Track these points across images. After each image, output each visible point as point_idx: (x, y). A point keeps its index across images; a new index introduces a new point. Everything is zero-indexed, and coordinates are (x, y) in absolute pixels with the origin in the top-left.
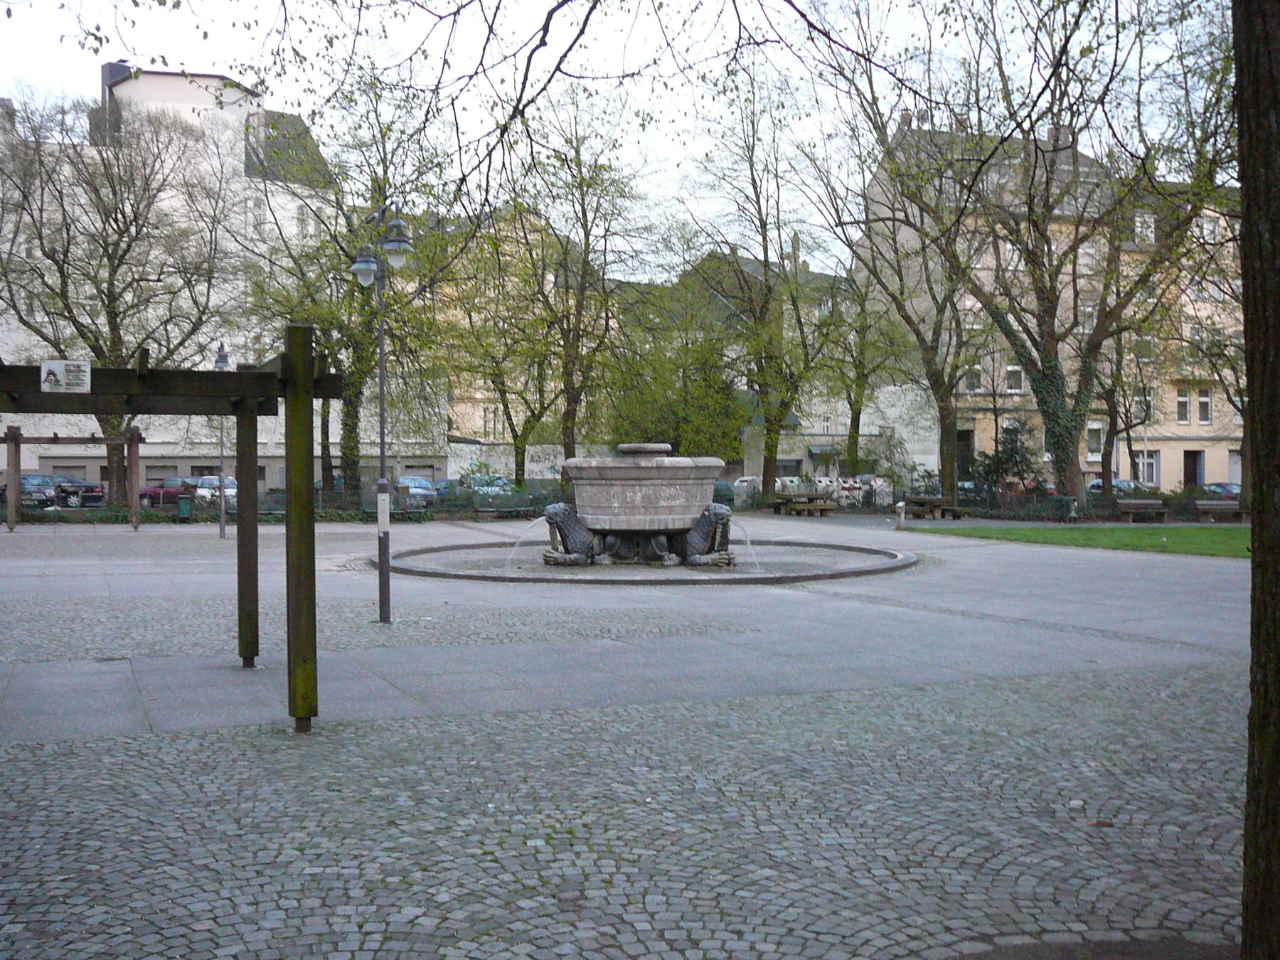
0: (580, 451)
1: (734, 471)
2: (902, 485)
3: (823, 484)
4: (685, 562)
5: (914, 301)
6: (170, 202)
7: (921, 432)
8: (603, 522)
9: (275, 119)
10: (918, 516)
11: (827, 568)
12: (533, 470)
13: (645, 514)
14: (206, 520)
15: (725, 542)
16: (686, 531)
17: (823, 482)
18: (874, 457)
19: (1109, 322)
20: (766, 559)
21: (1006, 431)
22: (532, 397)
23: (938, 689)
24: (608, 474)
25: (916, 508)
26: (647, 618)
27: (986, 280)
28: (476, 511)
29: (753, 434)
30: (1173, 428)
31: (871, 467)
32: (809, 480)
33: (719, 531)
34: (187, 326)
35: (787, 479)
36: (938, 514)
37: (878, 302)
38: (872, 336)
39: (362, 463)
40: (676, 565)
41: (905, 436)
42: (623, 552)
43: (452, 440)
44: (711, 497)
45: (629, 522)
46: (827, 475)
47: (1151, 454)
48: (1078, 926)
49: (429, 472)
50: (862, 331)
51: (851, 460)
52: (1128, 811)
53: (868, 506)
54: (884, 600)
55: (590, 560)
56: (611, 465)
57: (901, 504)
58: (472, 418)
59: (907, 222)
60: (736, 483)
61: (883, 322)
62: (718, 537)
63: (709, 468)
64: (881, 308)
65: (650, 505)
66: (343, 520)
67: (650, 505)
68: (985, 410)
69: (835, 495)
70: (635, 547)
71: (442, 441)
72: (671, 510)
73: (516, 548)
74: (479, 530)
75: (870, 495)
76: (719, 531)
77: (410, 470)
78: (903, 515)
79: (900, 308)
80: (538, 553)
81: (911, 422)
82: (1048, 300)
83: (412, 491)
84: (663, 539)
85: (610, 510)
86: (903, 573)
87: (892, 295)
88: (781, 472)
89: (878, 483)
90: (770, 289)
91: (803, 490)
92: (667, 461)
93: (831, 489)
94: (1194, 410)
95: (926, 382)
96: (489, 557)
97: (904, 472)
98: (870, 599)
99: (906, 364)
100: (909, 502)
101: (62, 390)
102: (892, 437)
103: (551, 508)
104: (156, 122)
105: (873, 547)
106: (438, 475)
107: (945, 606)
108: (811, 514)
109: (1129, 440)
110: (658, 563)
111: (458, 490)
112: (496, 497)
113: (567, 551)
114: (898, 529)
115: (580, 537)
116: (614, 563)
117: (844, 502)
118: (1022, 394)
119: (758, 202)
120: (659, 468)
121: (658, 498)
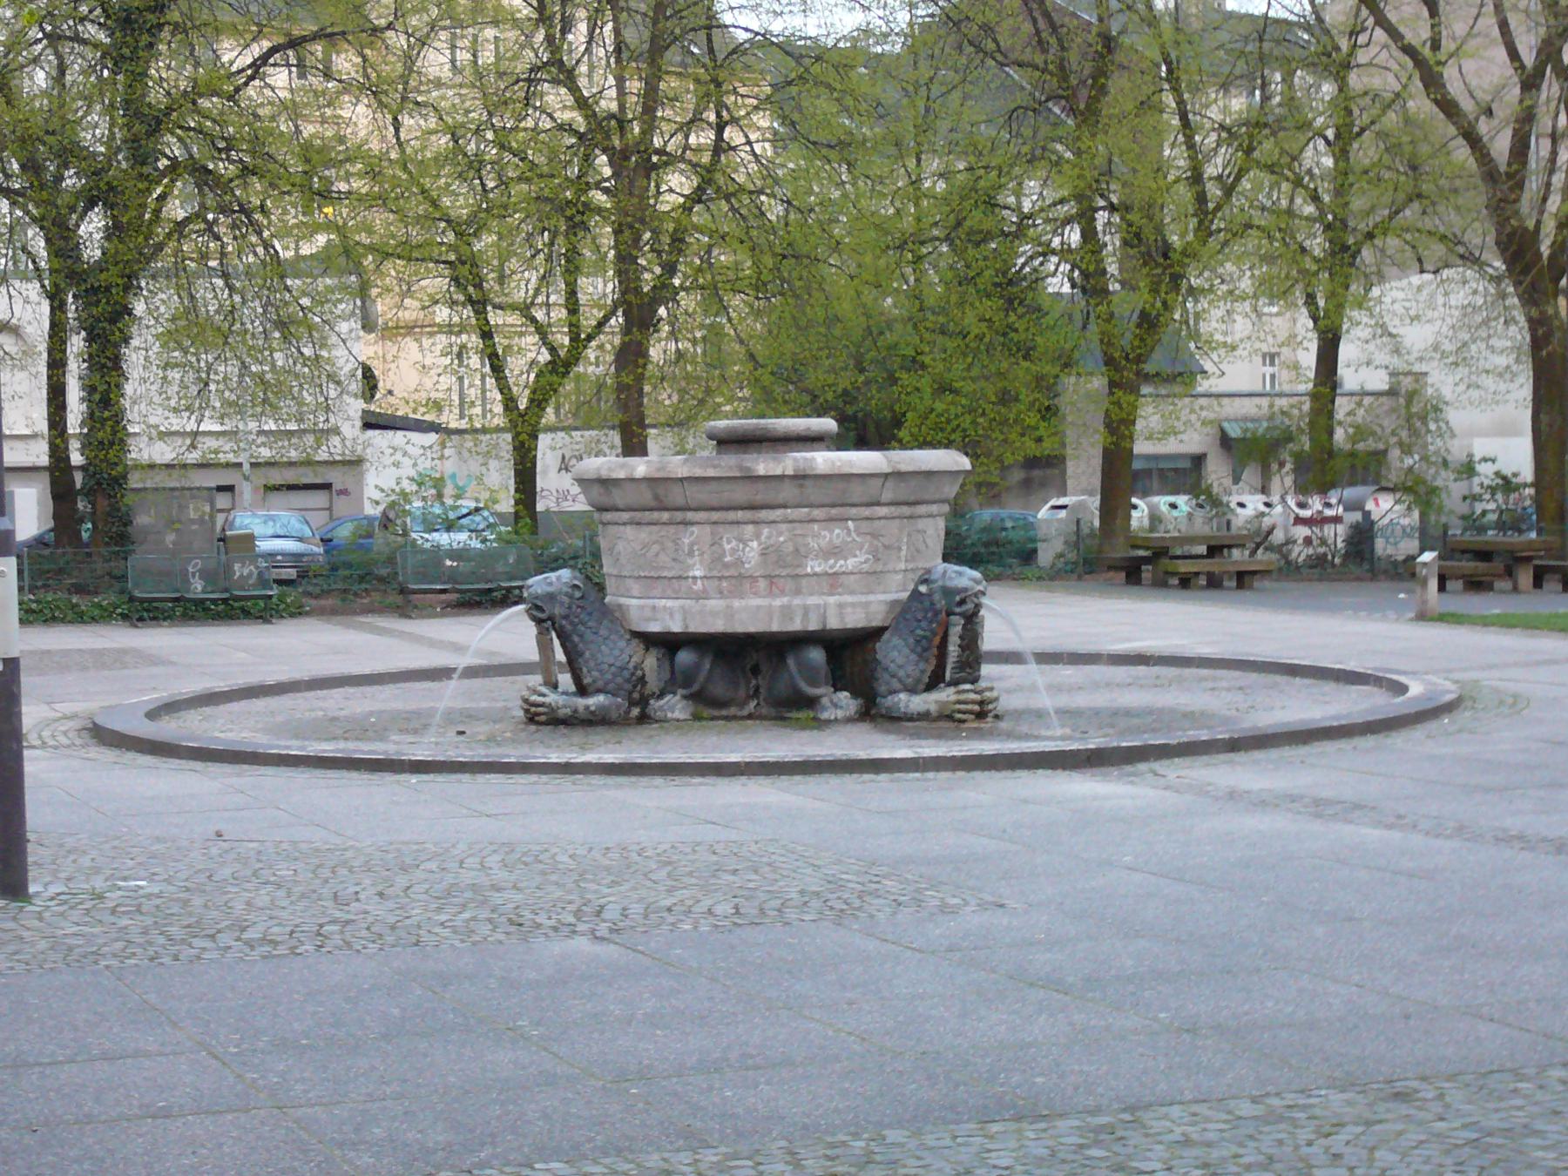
0: (657, 441)
2: (1440, 510)
3: (1248, 512)
4: (872, 712)
5: (1469, 65)
7: (1489, 382)
8: (668, 614)
10: (1476, 585)
11: (1226, 721)
12: (557, 489)
13: (771, 594)
15: (972, 659)
17: (1247, 505)
18: (1371, 444)
20: (1081, 700)
23: (1455, 1096)
24: (676, 496)
25: (1468, 565)
26: (718, 870)
28: (403, 591)
29: (1084, 391)
31: (1366, 468)
32: (1215, 502)
33: (956, 631)
35: (1162, 501)
36: (1525, 577)
37: (1379, 69)
38: (1365, 152)
39: (134, 481)
40: (849, 720)
41: (1447, 393)
42: (719, 689)
43: (371, 423)
45: (730, 614)
46: (1264, 490)
49: (320, 499)
50: (1341, 146)
51: (1314, 446)
53: (1359, 562)
54: (1352, 810)
55: (637, 710)
56: (683, 472)
57: (1428, 556)
58: (417, 370)
60: (1043, 513)
61: (1392, 118)
62: (953, 649)
63: (929, 474)
64: (1386, 83)
65: (782, 571)
66: (80, 618)
67: (782, 571)
69: (1278, 537)
70: (746, 673)
71: (351, 428)
72: (833, 580)
73: (453, 684)
74: (402, 635)
75: (1362, 535)
76: (956, 631)
77: (275, 498)
78: (1433, 584)
79: (1432, 81)
80: (510, 694)
81: (1459, 358)
83: (264, 545)
84: (817, 655)
85: (688, 586)
86: (1418, 733)
87: (1409, 50)
88: (1155, 484)
89: (1383, 507)
90: (1108, 42)
91: (1201, 527)
92: (823, 460)
93: (1267, 522)
95: (1499, 264)
96: (399, 705)
97: (1445, 479)
98: (1319, 807)
99: (1449, 219)
100: (1450, 551)
102: (1411, 396)
103: (538, 584)
105: (1352, 666)
106: (342, 506)
107: (1514, 824)
108: (1214, 583)
110: (802, 715)
111: (380, 541)
112: (459, 554)
113: (582, 690)
114: (1423, 616)
115: (612, 654)
116: (696, 717)
117: (1299, 553)
120: (800, 478)
121: (800, 554)
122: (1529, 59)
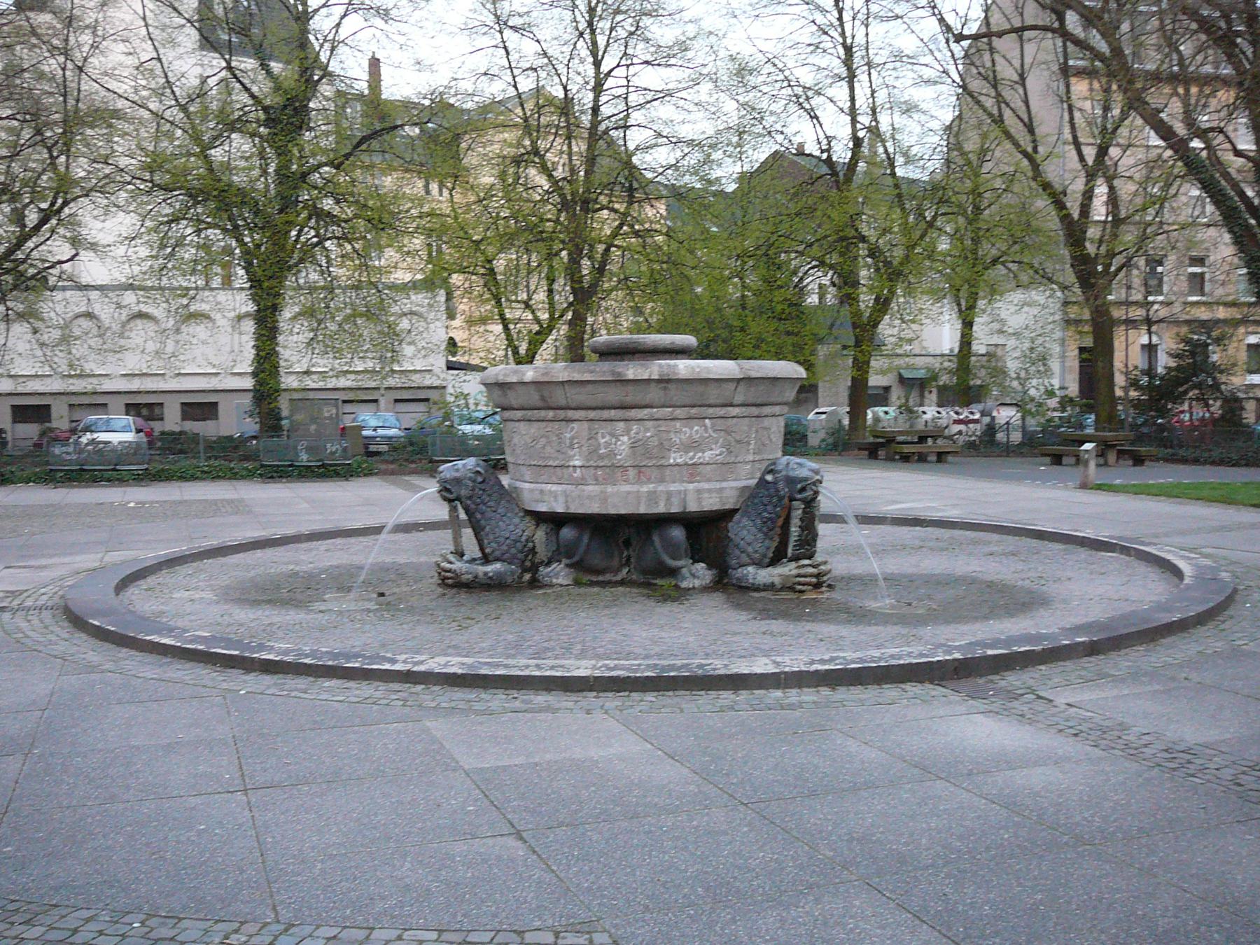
1: (806, 401)
8: (553, 497)
13: (639, 481)
14: (27, 481)
16: (724, 516)
24: (559, 397)
33: (797, 514)
40: (705, 589)
42: (596, 560)
44: (778, 439)
45: (604, 499)
51: (964, 381)
53: (988, 447)
60: (811, 416)
62: (794, 530)
67: (648, 462)
70: (622, 551)
72: (692, 471)
75: (991, 430)
76: (797, 514)
78: (1092, 464)
84: (678, 533)
85: (575, 474)
92: (684, 367)
108: (922, 458)
113: (486, 559)
114: (1084, 486)
116: (577, 583)
117: (961, 440)
120: (665, 381)
121: (664, 448)
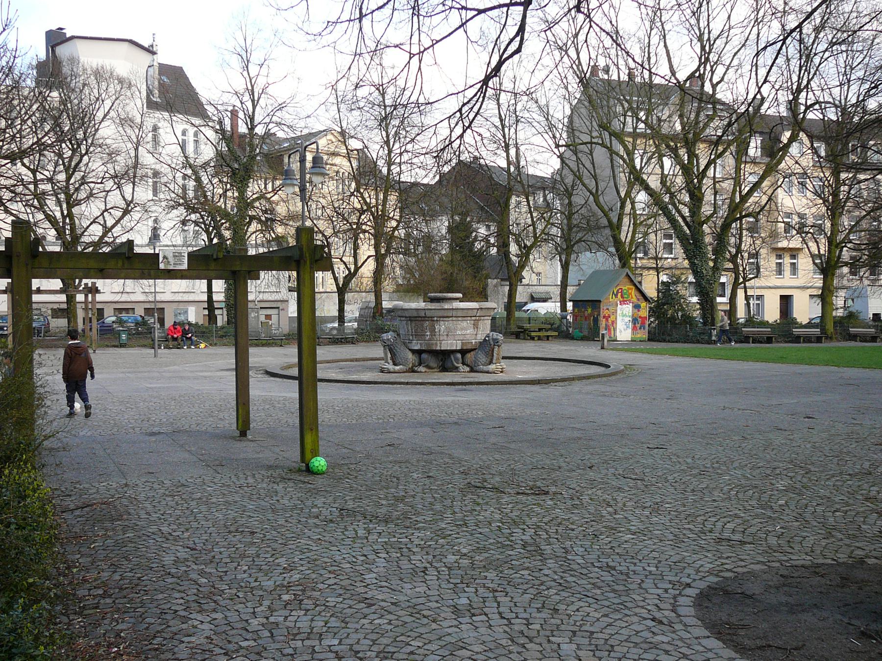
6: (108, 132)
9: (164, 69)
19: (736, 210)
21: (663, 283)
22: (349, 259)
27: (654, 182)
30: (774, 281)
34: (119, 214)
47: (759, 297)
48: (809, 558)
52: (812, 506)
59: (603, 145)
68: (649, 268)
82: (696, 199)
94: (787, 269)
101: (171, 268)
104: (98, 74)
108: (540, 338)
109: (745, 288)
113: (395, 364)
118: (677, 257)
119: (503, 130)
122: (623, 195)
